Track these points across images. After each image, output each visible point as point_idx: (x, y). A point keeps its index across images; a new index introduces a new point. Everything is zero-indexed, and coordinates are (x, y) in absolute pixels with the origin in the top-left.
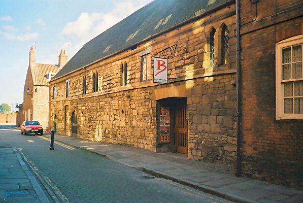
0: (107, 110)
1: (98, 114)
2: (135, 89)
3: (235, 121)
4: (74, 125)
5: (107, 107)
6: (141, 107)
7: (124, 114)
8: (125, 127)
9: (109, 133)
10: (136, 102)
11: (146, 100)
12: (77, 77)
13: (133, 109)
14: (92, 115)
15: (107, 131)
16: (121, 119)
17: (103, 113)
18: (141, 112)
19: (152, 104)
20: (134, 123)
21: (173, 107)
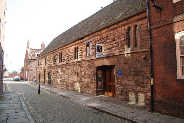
5: (67, 70)
6: (86, 71)
10: (84, 68)
13: (82, 72)
15: (67, 83)
17: (65, 74)
18: (86, 74)
19: (93, 69)
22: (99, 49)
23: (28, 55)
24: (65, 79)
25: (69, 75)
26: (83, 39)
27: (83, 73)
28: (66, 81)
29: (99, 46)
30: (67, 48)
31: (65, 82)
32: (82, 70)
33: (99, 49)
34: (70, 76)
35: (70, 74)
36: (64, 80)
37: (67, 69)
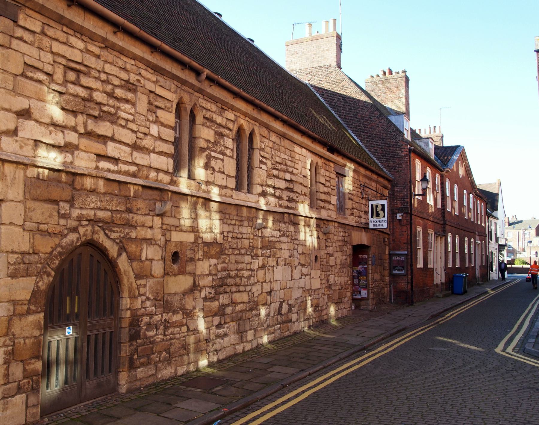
0: (286, 254)
1: (258, 263)
2: (332, 221)
3: (96, 204)
4: (366, 266)
5: (285, 246)
6: (339, 253)
7: (318, 265)
8: (319, 289)
9: (290, 310)
10: (334, 245)
11: (345, 242)
12: (105, 54)
13: (331, 255)
14: (232, 267)
15: (285, 307)
16: (314, 273)
17: (271, 262)
18: (339, 261)
19: (348, 249)
20: (332, 278)
21: (359, 250)
22: (377, 212)
23: (189, 159)
24: (277, 286)
25: (293, 268)
26: (332, 153)
27: (333, 258)
28: (279, 295)
29: (377, 206)
30: (287, 142)
31: (277, 305)
32: (330, 250)
33: (377, 212)
34: (297, 275)
35: (296, 263)
36: (269, 293)
37: (283, 239)
